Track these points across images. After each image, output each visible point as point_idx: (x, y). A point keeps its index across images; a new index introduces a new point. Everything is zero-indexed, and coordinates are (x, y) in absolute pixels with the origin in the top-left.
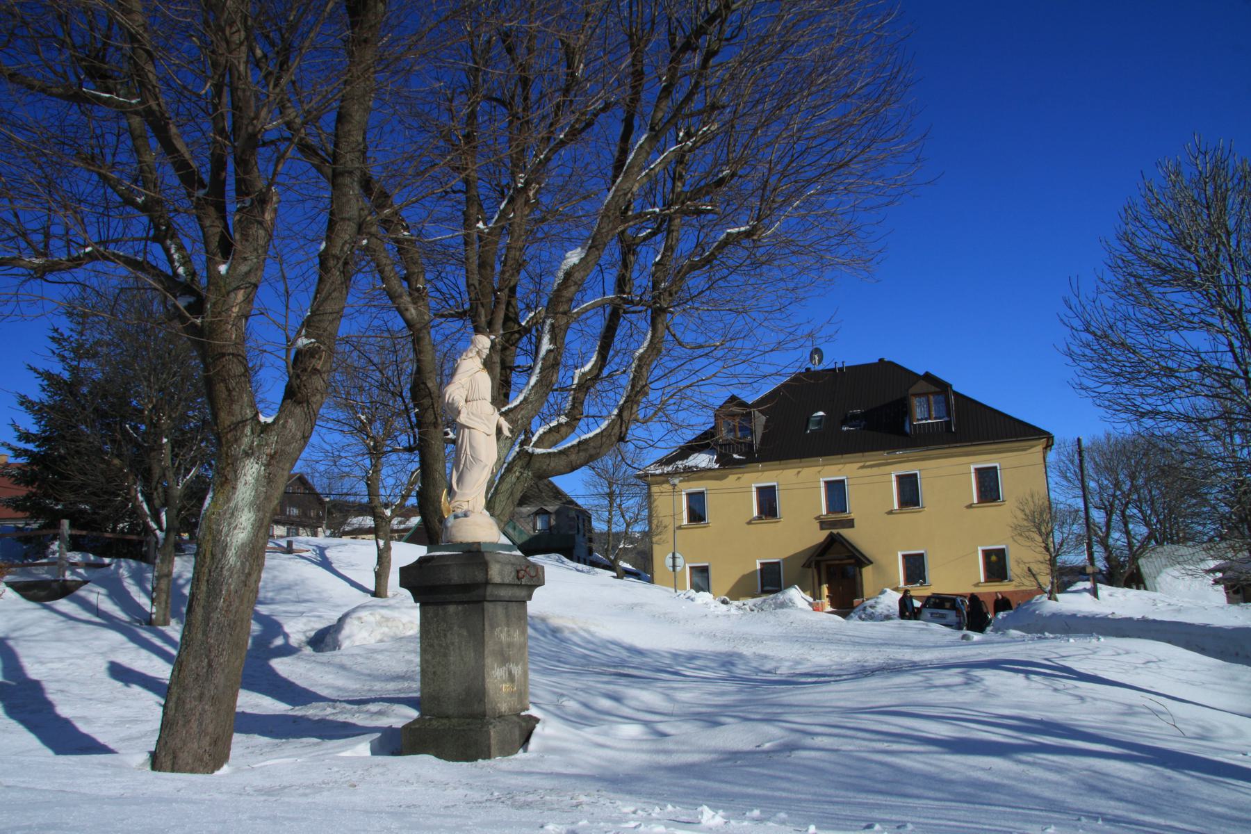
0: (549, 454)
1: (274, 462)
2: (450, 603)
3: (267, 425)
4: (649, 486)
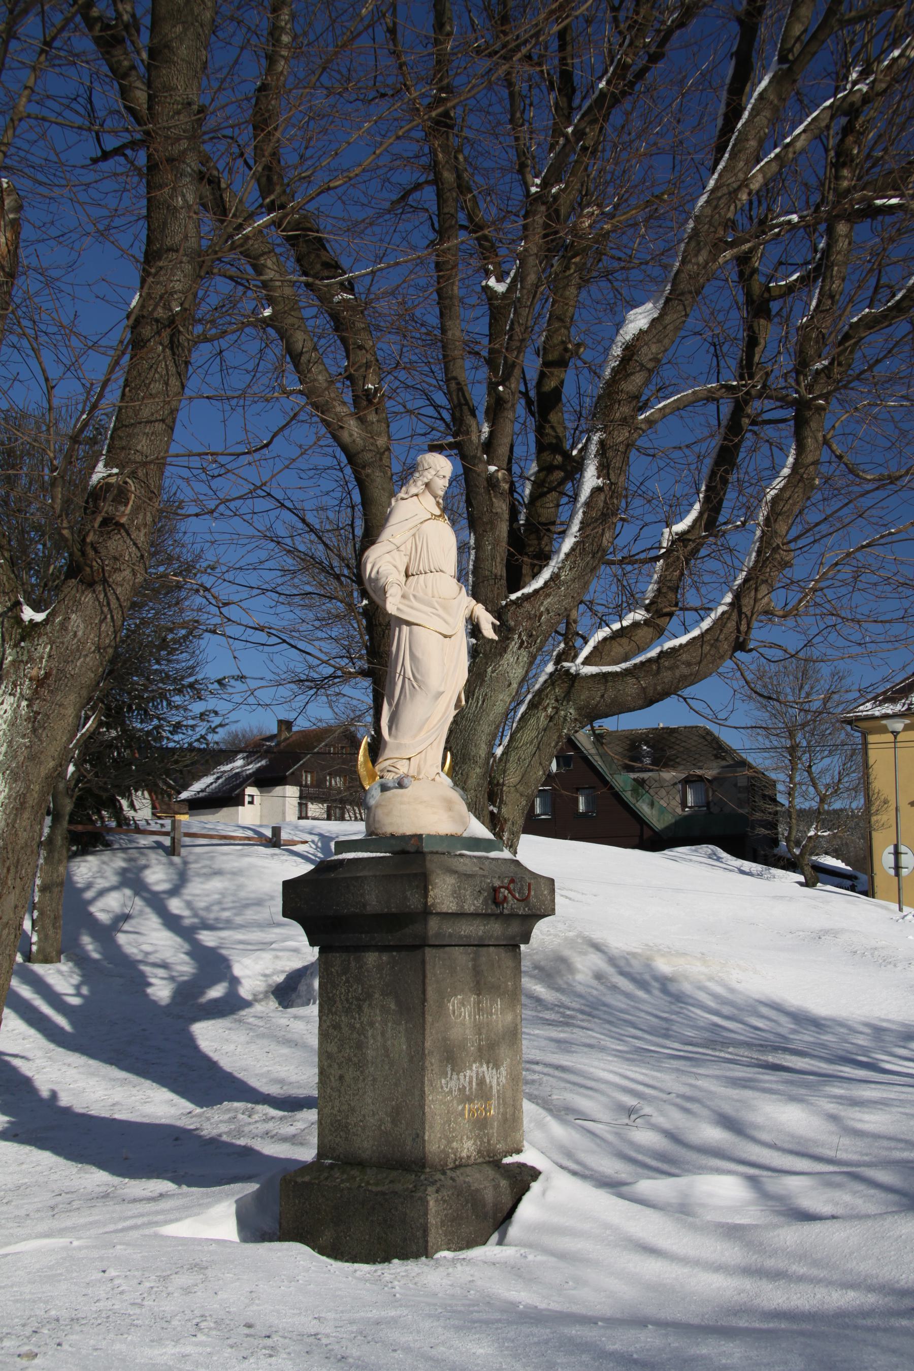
0: (605, 676)
1: (44, 692)
2: (367, 948)
3: (33, 624)
4: (864, 736)
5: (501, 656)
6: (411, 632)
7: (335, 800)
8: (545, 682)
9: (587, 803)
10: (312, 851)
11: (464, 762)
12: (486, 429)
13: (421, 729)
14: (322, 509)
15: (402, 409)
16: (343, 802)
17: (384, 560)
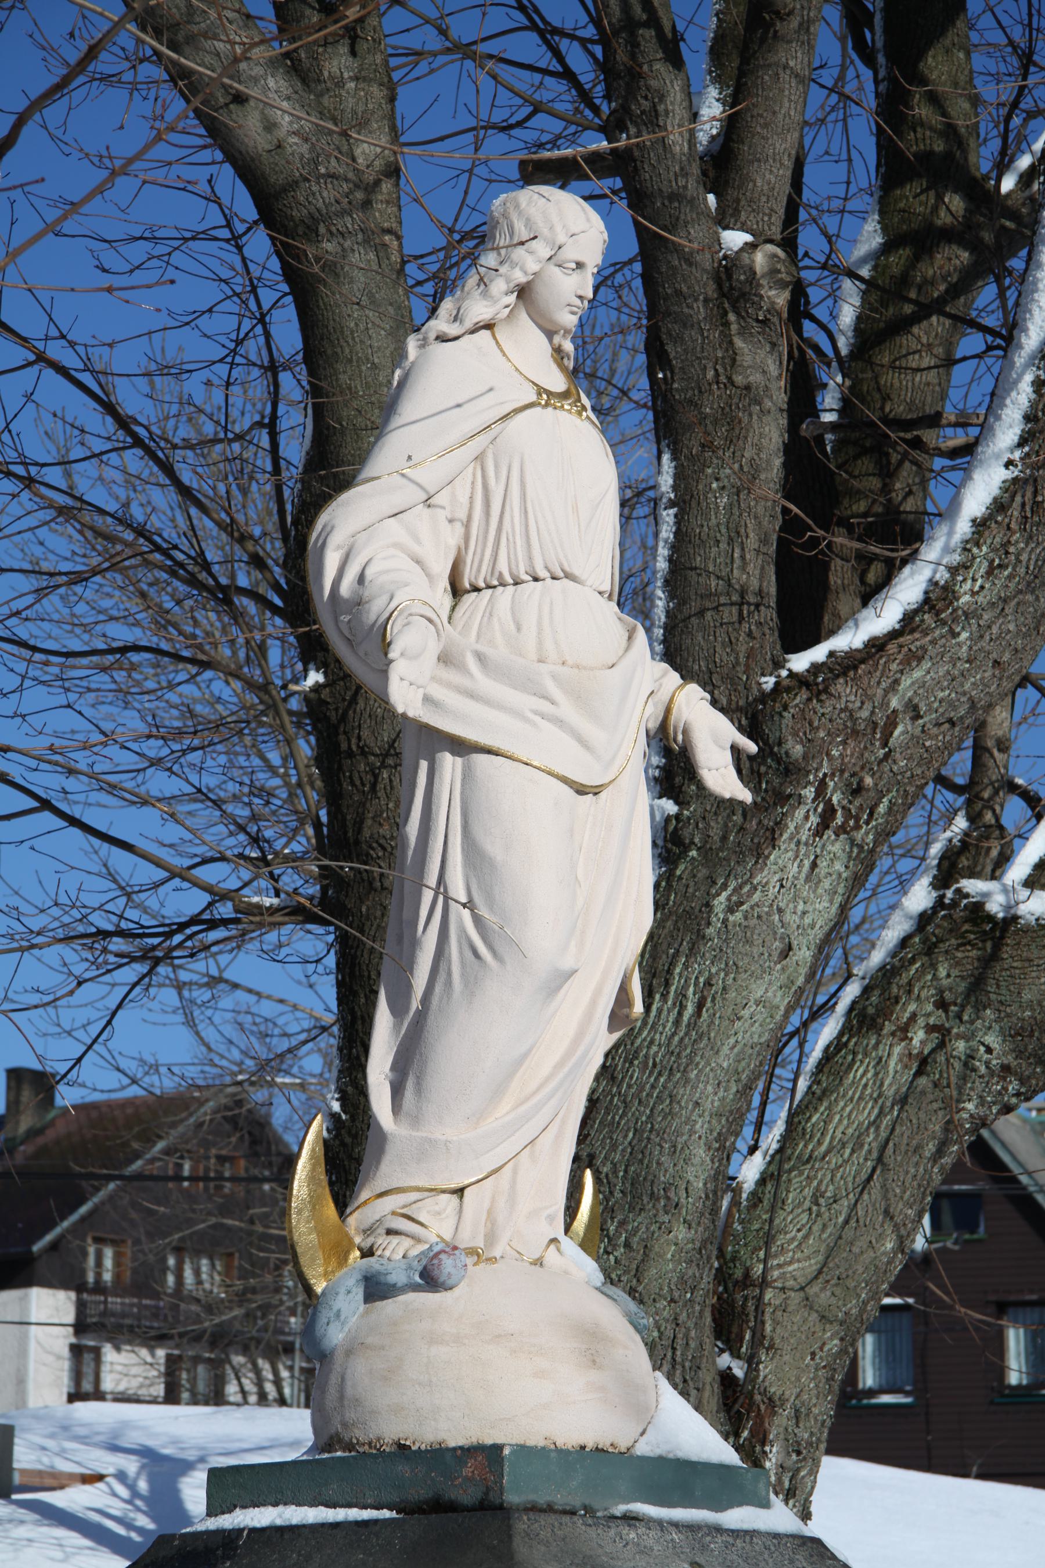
5: (759, 855)
6: (468, 775)
7: (197, 1338)
8: (904, 942)
9: (1038, 1355)
10: (117, 1508)
11: (635, 1207)
12: (712, 108)
13: (498, 1091)
14: (164, 370)
15: (432, 40)
16: (222, 1340)
17: (378, 540)
